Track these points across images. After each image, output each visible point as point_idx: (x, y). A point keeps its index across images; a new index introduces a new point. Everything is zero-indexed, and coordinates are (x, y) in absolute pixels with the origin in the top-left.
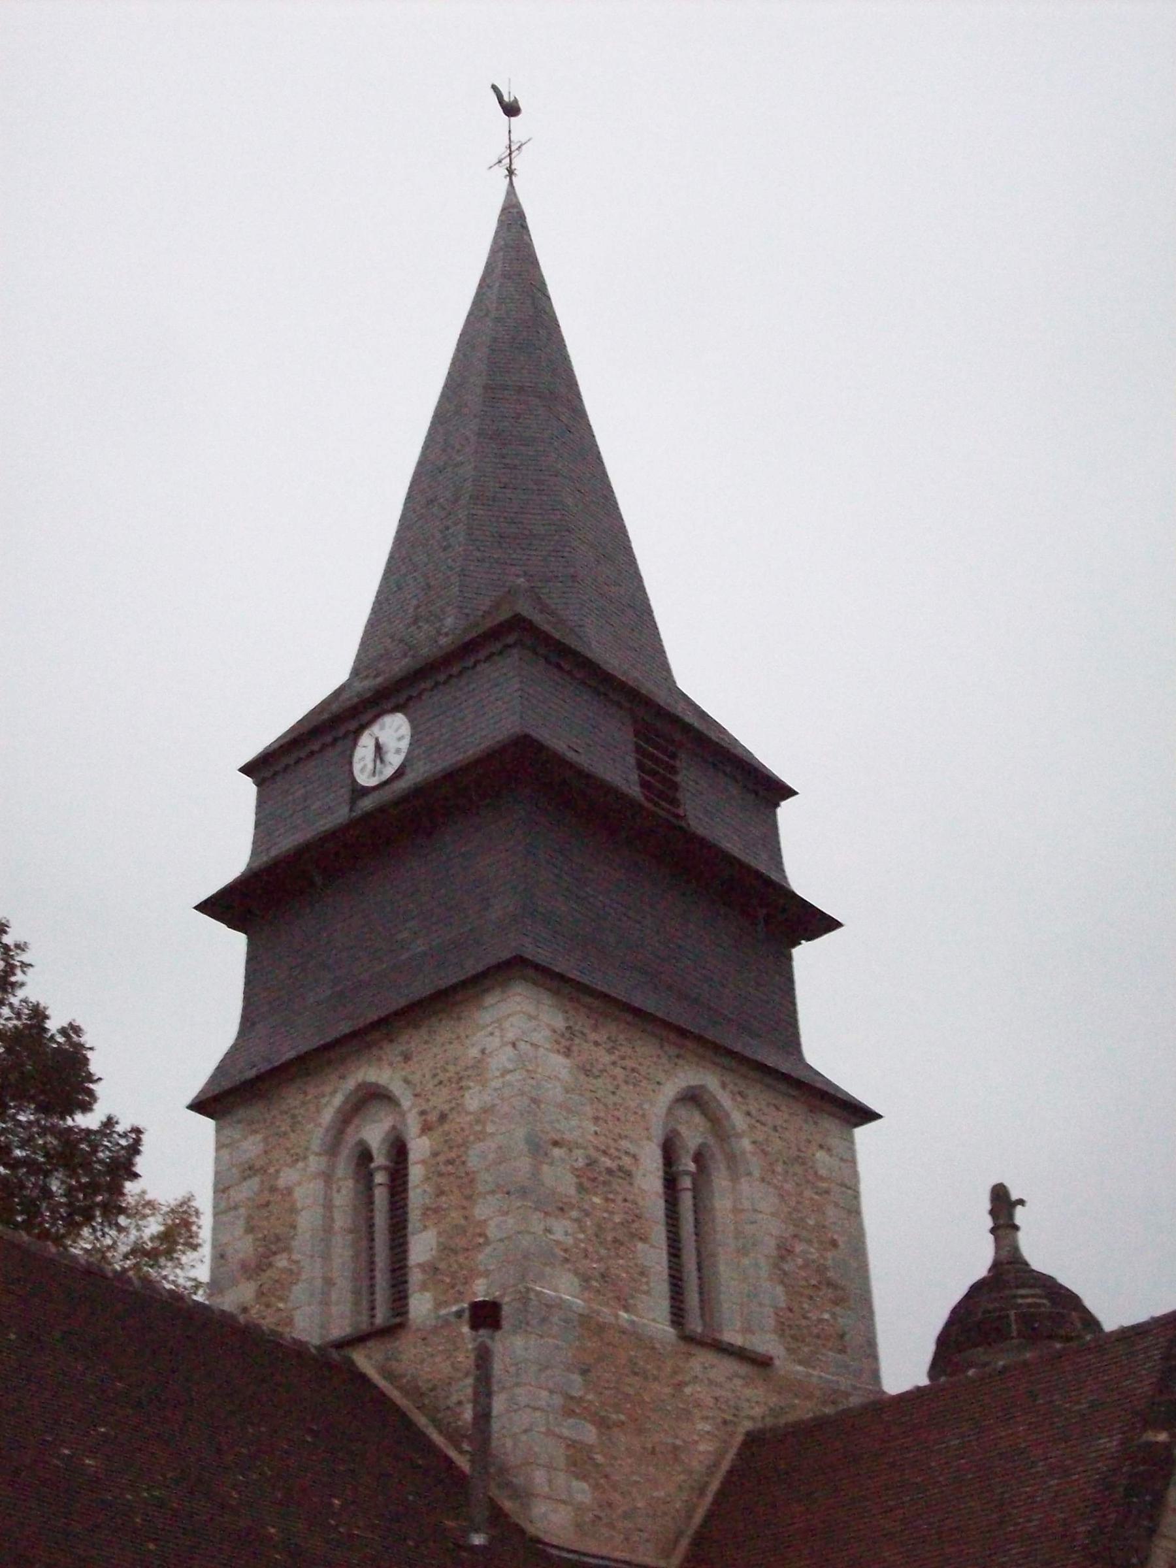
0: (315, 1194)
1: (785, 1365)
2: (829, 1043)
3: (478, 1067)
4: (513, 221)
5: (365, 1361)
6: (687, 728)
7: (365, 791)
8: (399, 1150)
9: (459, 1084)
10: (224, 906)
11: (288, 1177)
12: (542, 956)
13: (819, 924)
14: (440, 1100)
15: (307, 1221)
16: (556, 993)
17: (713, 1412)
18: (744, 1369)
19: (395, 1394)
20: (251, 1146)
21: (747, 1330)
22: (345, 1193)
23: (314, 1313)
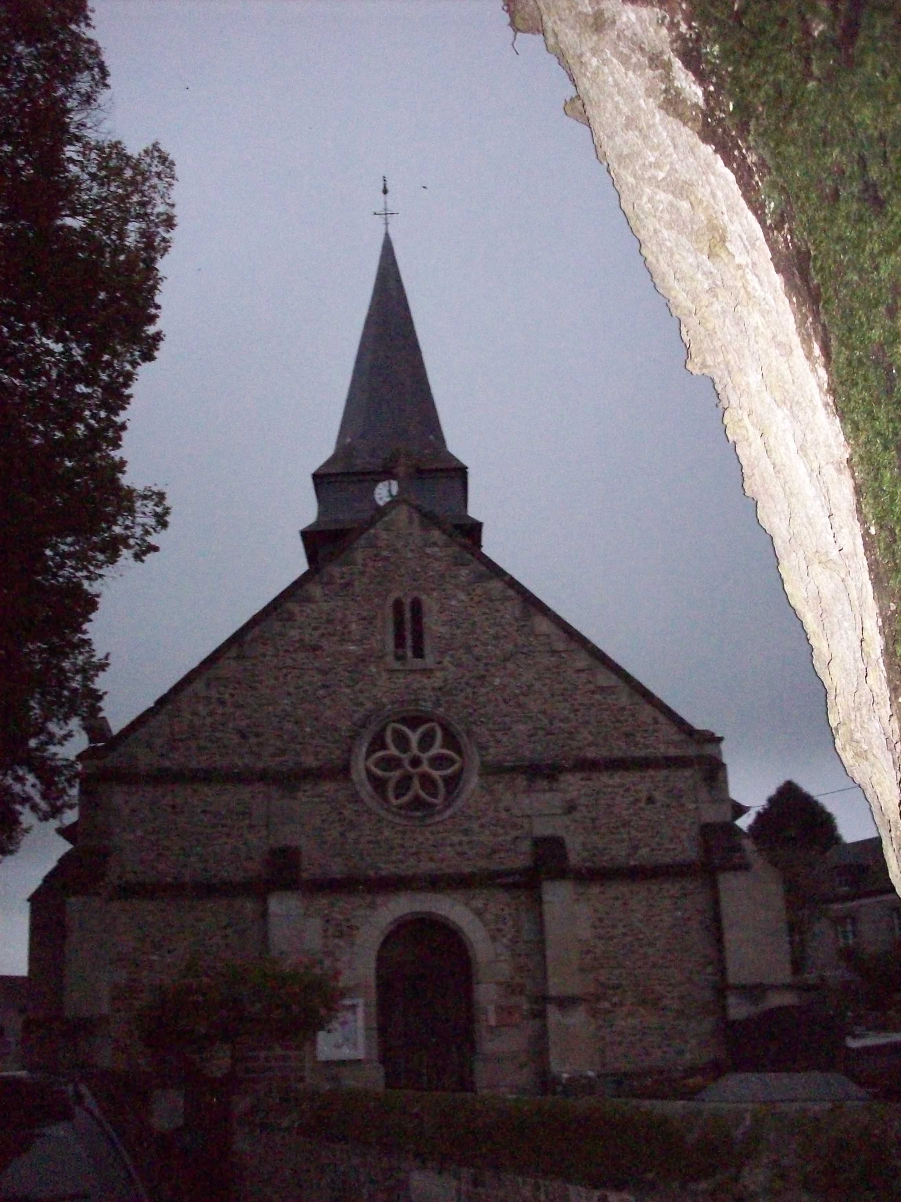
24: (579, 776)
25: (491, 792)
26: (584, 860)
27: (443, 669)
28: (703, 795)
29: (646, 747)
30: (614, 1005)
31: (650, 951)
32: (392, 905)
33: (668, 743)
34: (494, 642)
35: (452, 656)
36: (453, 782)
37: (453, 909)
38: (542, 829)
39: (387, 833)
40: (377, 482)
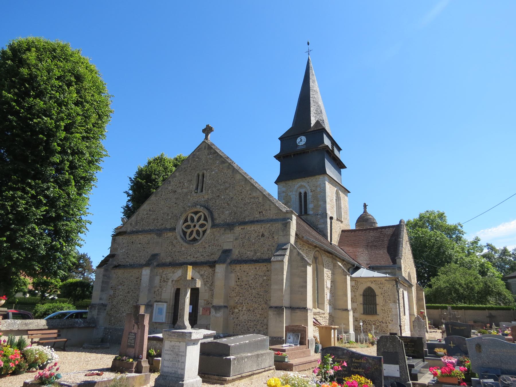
8: (305, 193)
11: (290, 194)
14: (314, 188)
20: (284, 189)
36: (204, 232)
38: (226, 247)
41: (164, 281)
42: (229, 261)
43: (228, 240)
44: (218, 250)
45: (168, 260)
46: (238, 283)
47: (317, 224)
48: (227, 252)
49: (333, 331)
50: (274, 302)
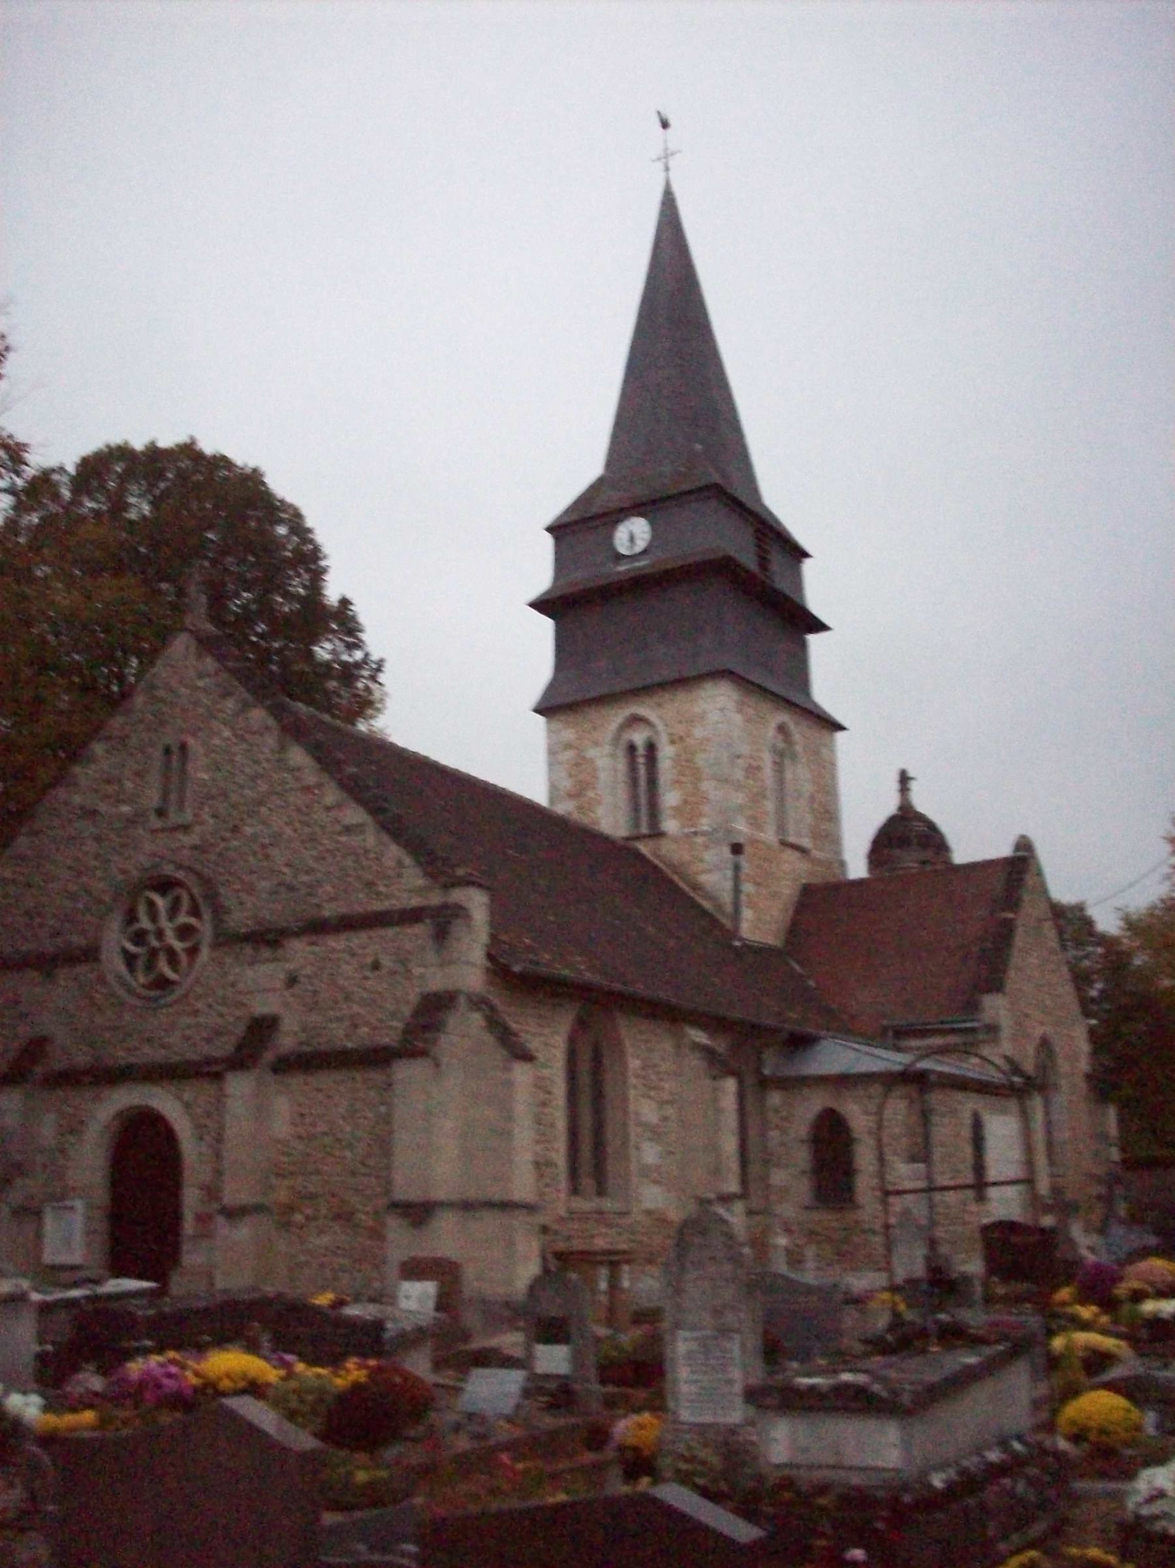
0: (607, 765)
1: (816, 853)
2: (825, 692)
3: (702, 717)
4: (669, 205)
5: (644, 848)
6: (771, 528)
7: (619, 557)
8: (651, 748)
9: (691, 722)
10: (541, 605)
11: (591, 753)
12: (739, 670)
13: (819, 626)
14: (680, 730)
15: (603, 776)
16: (732, 681)
17: (790, 874)
18: (797, 854)
19: (661, 865)
20: (569, 734)
21: (799, 835)
22: (622, 765)
23: (610, 817)
24: (305, 939)
25: (221, 964)
26: (301, 1043)
27: (202, 823)
28: (431, 956)
29: (387, 897)
30: (307, 1218)
31: (348, 1154)
32: (115, 1096)
33: (419, 891)
34: (251, 784)
35: (210, 807)
36: (193, 952)
37: (165, 1102)
38: (262, 1006)
39: (127, 1017)
40: (618, 521)
41: (72, 1132)
42: (268, 1056)
43: (261, 985)
44: (238, 1018)
45: (82, 1058)
46: (301, 1130)
47: (694, 868)
48: (262, 1028)
49: (604, 1272)
50: (405, 1191)
